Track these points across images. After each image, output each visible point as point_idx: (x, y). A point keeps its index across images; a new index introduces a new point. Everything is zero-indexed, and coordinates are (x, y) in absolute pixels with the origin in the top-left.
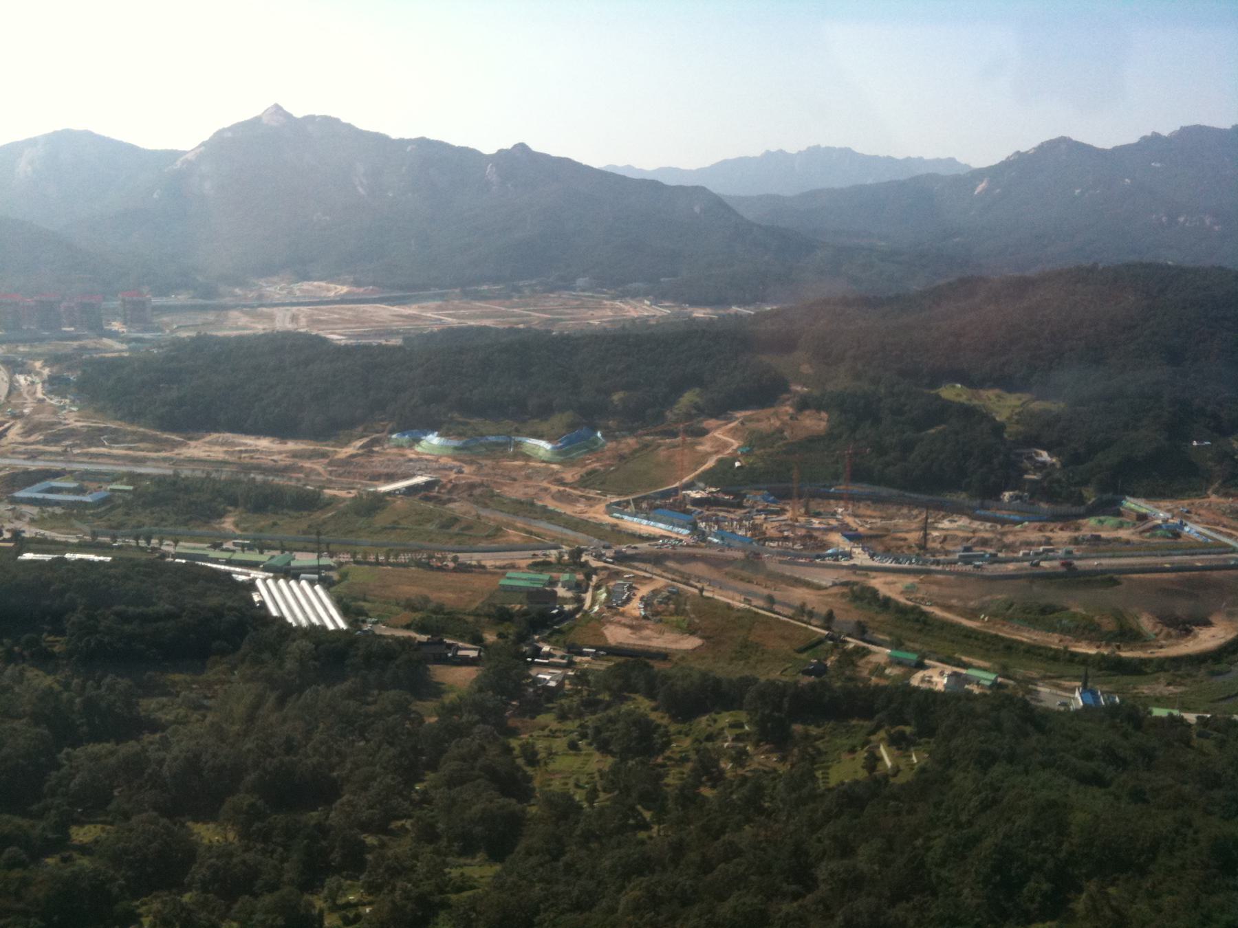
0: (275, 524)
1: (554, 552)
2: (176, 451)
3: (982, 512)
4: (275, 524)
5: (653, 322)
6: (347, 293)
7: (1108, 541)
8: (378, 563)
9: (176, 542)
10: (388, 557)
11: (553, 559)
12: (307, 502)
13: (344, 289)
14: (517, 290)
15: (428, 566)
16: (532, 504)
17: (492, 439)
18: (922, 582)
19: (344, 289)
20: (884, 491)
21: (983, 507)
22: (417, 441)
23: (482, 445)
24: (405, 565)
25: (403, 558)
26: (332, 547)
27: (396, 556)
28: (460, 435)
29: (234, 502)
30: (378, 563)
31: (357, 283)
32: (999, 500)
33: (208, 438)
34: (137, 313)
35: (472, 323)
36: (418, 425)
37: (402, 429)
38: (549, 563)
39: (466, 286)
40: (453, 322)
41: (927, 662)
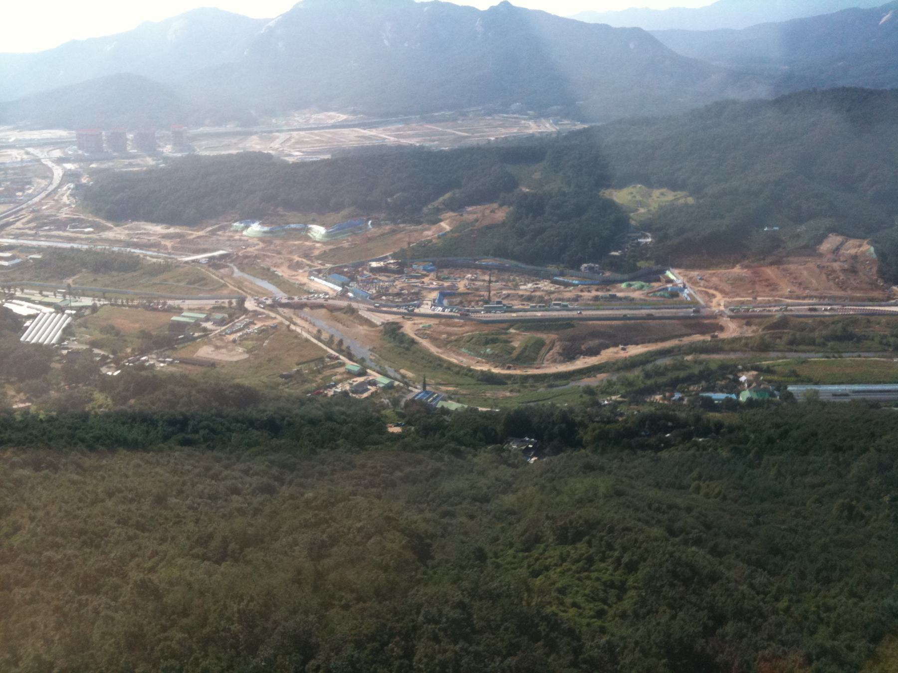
0: (95, 280)
1: (227, 301)
2: (498, 263)
3: (561, 279)
4: (95, 280)
5: (510, 139)
6: (345, 120)
7: (620, 299)
8: (123, 305)
9: (22, 290)
10: (127, 302)
11: (227, 305)
12: (131, 265)
13: (343, 117)
14: (464, 115)
15: (148, 308)
16: (269, 269)
17: (293, 226)
18: (440, 323)
19: (343, 117)
20: (508, 263)
21: (562, 274)
22: (247, 227)
23: (284, 230)
24: (136, 307)
25: (136, 303)
26: (107, 295)
27: (132, 300)
28: (272, 223)
29: (84, 264)
30: (123, 305)
31: (354, 113)
32: (579, 269)
33: (129, 225)
34: (178, 139)
35: (223, 153)
36: (249, 217)
37: (241, 220)
38: (224, 308)
39: (425, 113)
40: (415, 142)
41: (369, 371)
